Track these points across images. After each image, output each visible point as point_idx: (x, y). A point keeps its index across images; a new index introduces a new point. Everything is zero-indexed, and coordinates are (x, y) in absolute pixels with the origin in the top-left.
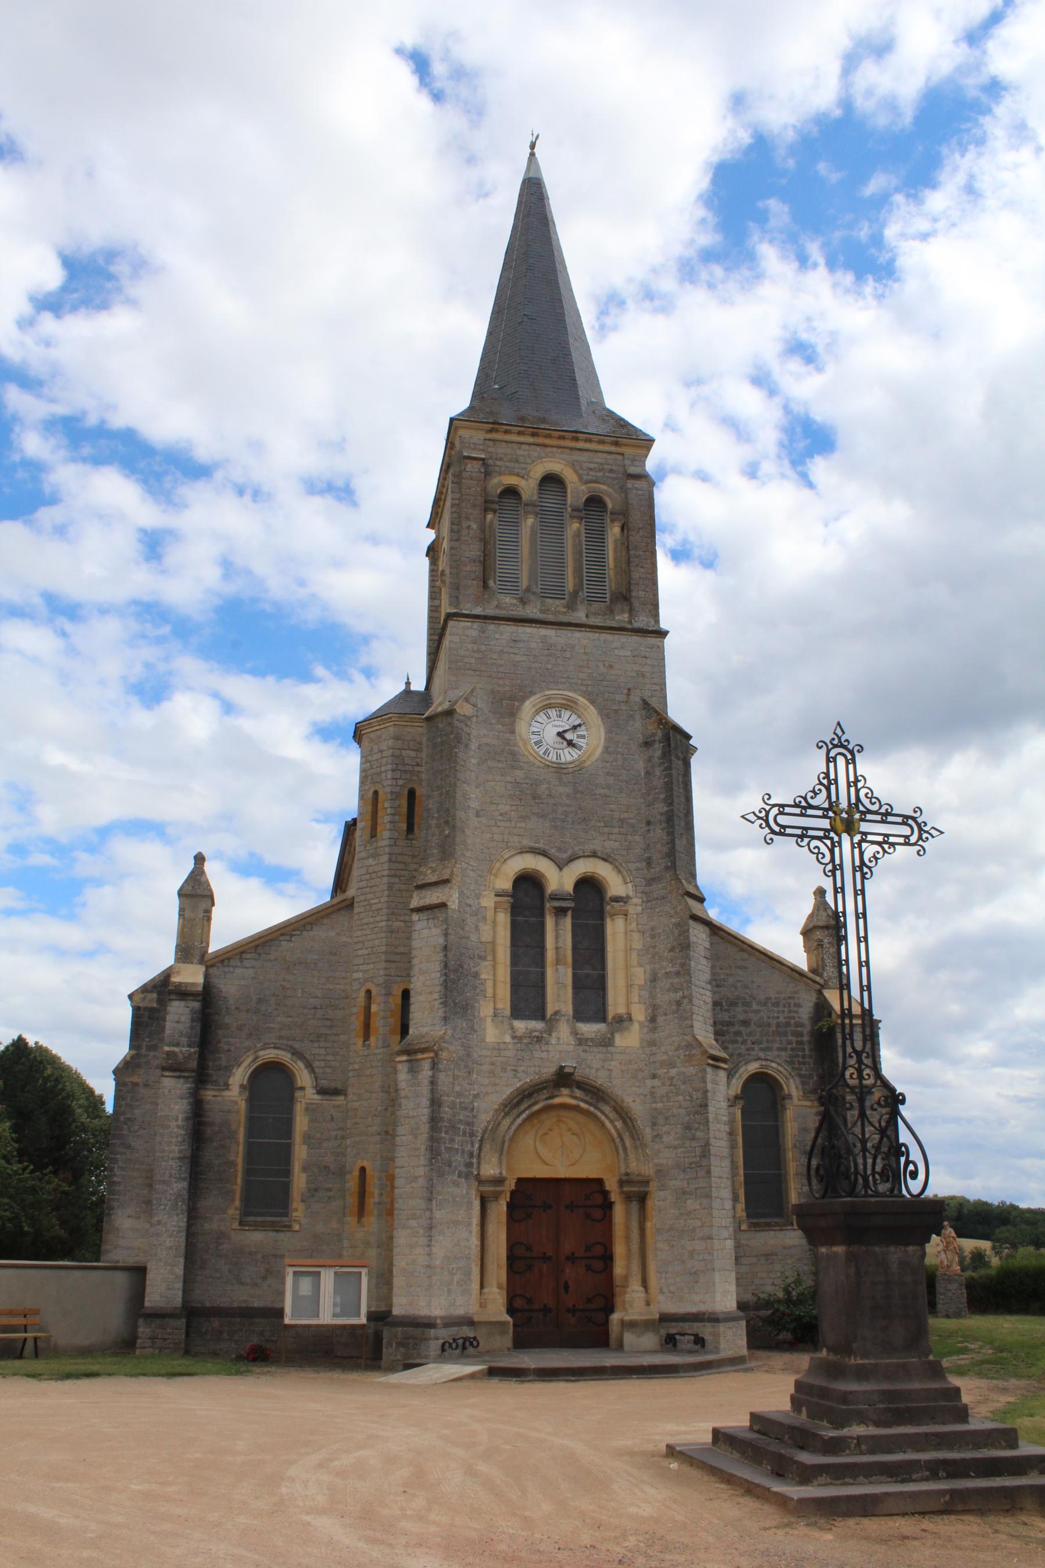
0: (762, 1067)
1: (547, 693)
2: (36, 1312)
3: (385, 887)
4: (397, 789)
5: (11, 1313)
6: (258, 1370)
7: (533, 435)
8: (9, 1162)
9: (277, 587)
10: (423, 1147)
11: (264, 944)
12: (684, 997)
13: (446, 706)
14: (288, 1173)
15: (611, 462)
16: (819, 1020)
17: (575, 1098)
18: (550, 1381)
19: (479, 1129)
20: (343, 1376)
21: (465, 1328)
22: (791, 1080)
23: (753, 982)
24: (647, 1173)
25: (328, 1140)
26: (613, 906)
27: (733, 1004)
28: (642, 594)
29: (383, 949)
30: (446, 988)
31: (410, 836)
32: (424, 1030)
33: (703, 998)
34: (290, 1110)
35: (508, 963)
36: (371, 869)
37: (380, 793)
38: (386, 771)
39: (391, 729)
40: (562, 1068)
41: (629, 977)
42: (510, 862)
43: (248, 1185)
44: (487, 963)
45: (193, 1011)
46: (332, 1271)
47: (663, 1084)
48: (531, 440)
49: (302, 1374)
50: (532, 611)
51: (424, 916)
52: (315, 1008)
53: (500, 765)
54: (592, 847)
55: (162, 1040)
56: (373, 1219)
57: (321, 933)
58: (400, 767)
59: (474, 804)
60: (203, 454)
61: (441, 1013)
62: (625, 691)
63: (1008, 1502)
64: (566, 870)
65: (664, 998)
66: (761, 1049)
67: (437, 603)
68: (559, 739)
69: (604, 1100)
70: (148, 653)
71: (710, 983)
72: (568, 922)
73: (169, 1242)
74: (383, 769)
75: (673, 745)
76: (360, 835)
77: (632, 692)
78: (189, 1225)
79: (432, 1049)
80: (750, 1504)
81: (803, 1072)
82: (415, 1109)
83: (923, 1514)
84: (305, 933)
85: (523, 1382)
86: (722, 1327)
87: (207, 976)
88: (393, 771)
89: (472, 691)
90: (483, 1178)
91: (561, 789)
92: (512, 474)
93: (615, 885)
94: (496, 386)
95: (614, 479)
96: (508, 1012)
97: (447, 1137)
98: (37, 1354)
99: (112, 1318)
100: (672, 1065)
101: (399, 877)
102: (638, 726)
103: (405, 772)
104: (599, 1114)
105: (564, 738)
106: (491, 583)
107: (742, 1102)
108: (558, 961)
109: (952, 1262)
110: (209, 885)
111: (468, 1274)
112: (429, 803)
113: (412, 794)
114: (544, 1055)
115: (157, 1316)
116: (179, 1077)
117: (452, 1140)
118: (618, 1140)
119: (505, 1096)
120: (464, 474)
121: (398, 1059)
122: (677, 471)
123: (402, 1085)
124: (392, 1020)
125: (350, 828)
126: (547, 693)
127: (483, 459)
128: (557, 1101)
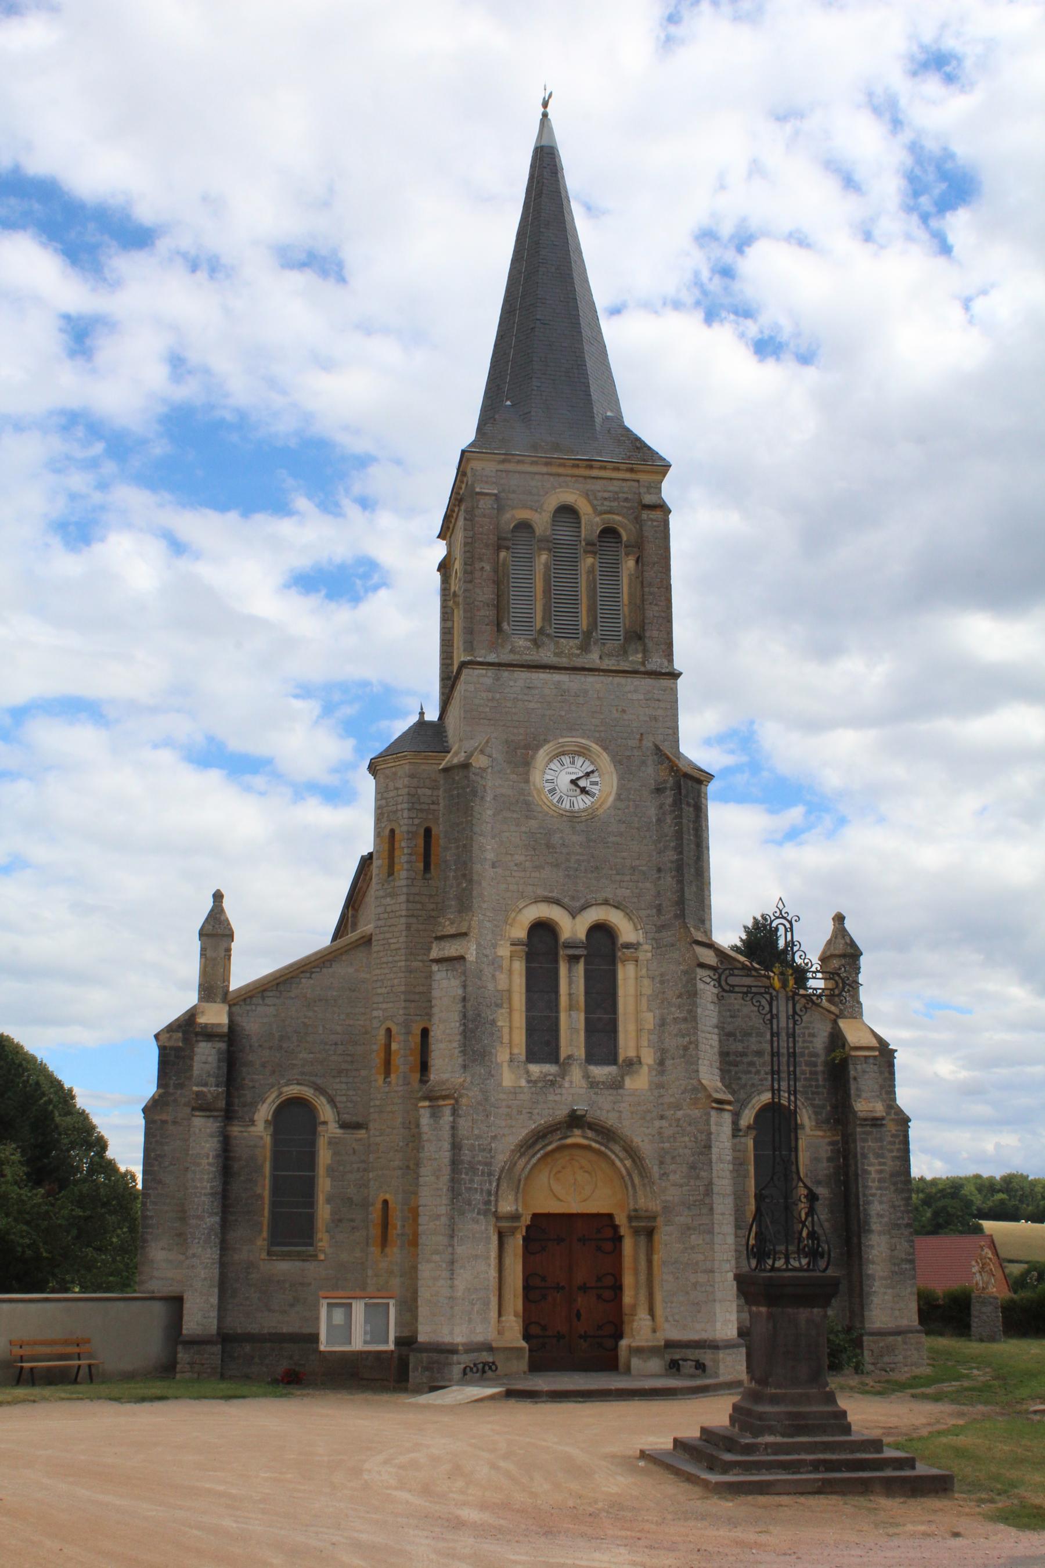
1: (561, 741)
2: (88, 1341)
3: (403, 927)
4: (414, 829)
5: (66, 1342)
6: (299, 1392)
7: (547, 464)
9: (240, 389)
11: (285, 982)
12: (690, 1043)
13: (461, 758)
15: (626, 489)
16: (834, 1051)
17: (587, 1138)
18: (560, 1402)
20: (349, 1397)
21: (484, 1353)
24: (654, 1209)
26: (624, 953)
27: (747, 1034)
28: (655, 634)
29: (403, 988)
30: (465, 1037)
31: (428, 876)
32: (445, 1076)
33: (709, 1043)
34: (313, 1143)
35: (524, 1009)
36: (389, 909)
38: (402, 810)
39: (407, 767)
40: (574, 1111)
41: (638, 1021)
42: (525, 911)
43: (274, 1216)
44: (504, 1011)
47: (670, 1125)
48: (544, 470)
49: (339, 1396)
50: (546, 655)
51: (444, 966)
52: (336, 1044)
53: (515, 816)
54: (604, 895)
55: (190, 1078)
56: (396, 1250)
57: (342, 970)
58: (417, 806)
59: (490, 856)
60: (145, 213)
61: (460, 1061)
62: (638, 737)
63: (864, 1488)
64: (579, 919)
67: (449, 624)
70: (78, 481)
71: (717, 1027)
72: (581, 967)
74: (399, 807)
75: (683, 792)
76: (377, 867)
77: (644, 737)
78: (221, 1256)
79: (453, 1097)
80: (686, 1486)
81: (817, 1102)
82: (436, 1152)
83: (802, 1494)
84: (324, 970)
85: (536, 1402)
86: (721, 1354)
87: (231, 1015)
88: (409, 810)
89: (487, 742)
90: (501, 1215)
91: (575, 838)
92: (525, 507)
93: (627, 931)
94: (508, 403)
95: (629, 508)
96: (523, 1057)
97: (467, 1178)
98: (91, 1378)
100: (678, 1107)
101: (417, 917)
102: (651, 773)
103: (421, 810)
104: (609, 1153)
105: (577, 785)
106: (505, 626)
107: (753, 1133)
108: (571, 1008)
109: (988, 1283)
110: (229, 924)
111: (487, 1304)
112: (445, 852)
113: (428, 832)
114: (557, 1098)
115: (196, 1342)
117: (472, 1181)
118: (627, 1178)
119: (521, 1138)
120: (478, 512)
121: (421, 1104)
122: (766, 234)
124: (411, 1058)
125: (366, 861)
126: (561, 741)
127: (495, 495)
128: (569, 1141)
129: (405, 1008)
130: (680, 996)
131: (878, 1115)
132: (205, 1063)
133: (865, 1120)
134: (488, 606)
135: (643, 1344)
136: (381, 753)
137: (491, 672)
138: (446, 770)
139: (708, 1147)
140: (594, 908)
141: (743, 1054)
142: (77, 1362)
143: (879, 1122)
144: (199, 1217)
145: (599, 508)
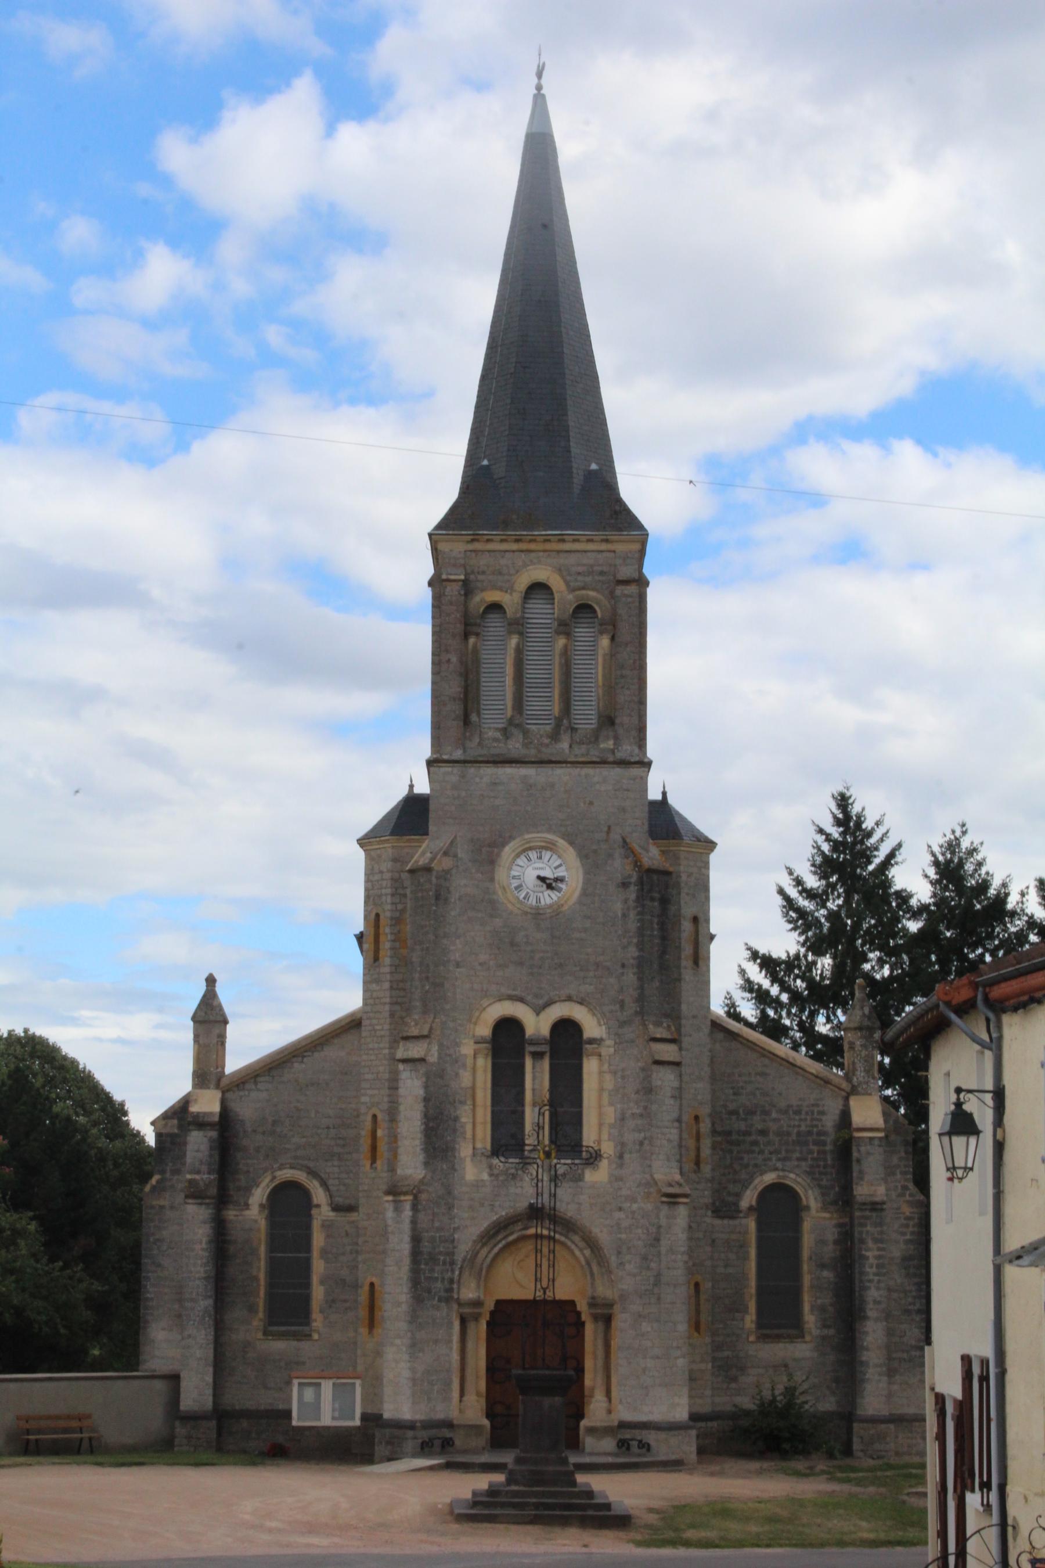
0: (779, 1177)
1: (527, 836)
3: (387, 1014)
5: (69, 1417)
8: (37, 1261)
10: (405, 1278)
12: (645, 1138)
14: (308, 1285)
19: (459, 1258)
22: (810, 1192)
23: (773, 1089)
25: (343, 1254)
32: (409, 1172)
34: (308, 1227)
35: (489, 1102)
36: (375, 995)
37: (382, 917)
38: (386, 895)
41: (601, 1115)
42: (490, 1010)
43: (271, 1297)
44: (467, 1108)
45: (211, 1140)
46: (330, 1382)
47: (627, 1217)
48: (515, 546)
53: (480, 915)
55: (184, 1164)
62: (606, 829)
64: (543, 1015)
65: (630, 1137)
66: (779, 1160)
68: (539, 883)
69: (575, 1232)
72: (546, 1064)
73: (198, 1353)
81: (824, 1183)
84: (316, 1054)
87: (223, 1102)
88: (393, 895)
92: (495, 587)
93: (591, 1027)
98: (92, 1451)
99: (153, 1418)
100: (634, 1200)
104: (569, 1243)
111: (448, 1384)
114: (519, 1191)
116: (200, 1204)
117: (432, 1270)
119: (482, 1229)
123: (390, 1222)
129: (389, 1096)
130: (637, 1092)
131: (877, 1199)
132: (197, 1151)
133: (864, 1204)
134: (454, 699)
135: (598, 1424)
136: (366, 835)
137: (456, 770)
138: (412, 871)
139: (657, 1240)
140: (558, 1004)
141: (747, 1133)
142: (80, 1435)
143: (879, 1207)
144: (192, 1300)
145: (572, 584)
